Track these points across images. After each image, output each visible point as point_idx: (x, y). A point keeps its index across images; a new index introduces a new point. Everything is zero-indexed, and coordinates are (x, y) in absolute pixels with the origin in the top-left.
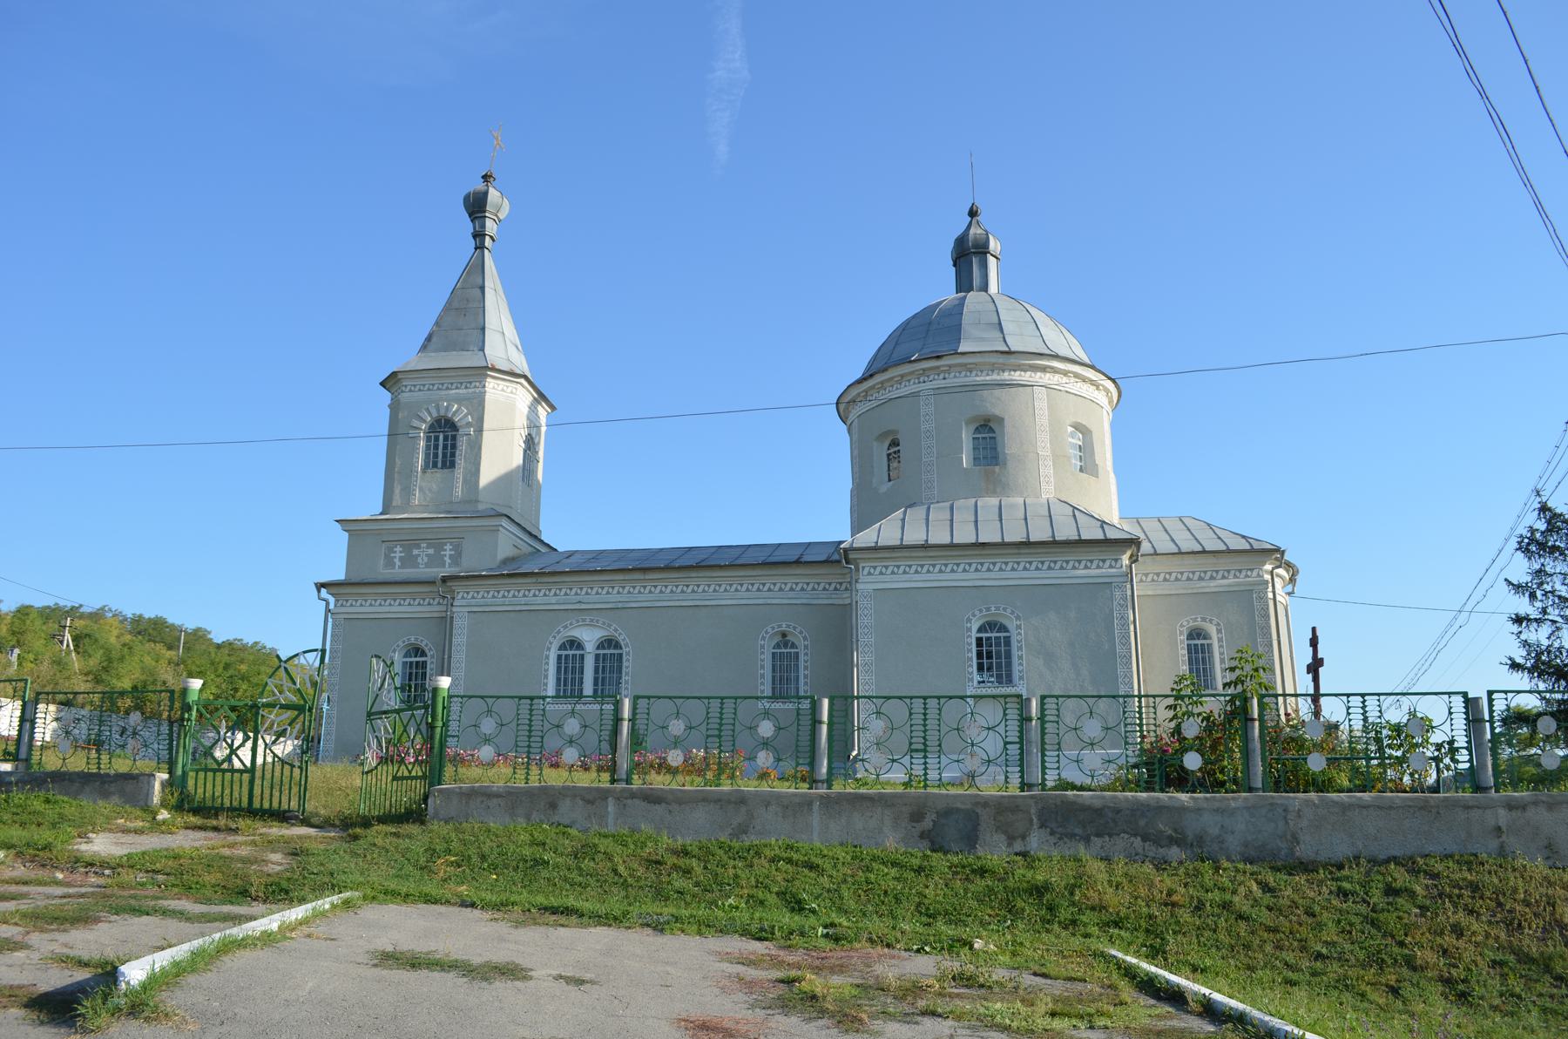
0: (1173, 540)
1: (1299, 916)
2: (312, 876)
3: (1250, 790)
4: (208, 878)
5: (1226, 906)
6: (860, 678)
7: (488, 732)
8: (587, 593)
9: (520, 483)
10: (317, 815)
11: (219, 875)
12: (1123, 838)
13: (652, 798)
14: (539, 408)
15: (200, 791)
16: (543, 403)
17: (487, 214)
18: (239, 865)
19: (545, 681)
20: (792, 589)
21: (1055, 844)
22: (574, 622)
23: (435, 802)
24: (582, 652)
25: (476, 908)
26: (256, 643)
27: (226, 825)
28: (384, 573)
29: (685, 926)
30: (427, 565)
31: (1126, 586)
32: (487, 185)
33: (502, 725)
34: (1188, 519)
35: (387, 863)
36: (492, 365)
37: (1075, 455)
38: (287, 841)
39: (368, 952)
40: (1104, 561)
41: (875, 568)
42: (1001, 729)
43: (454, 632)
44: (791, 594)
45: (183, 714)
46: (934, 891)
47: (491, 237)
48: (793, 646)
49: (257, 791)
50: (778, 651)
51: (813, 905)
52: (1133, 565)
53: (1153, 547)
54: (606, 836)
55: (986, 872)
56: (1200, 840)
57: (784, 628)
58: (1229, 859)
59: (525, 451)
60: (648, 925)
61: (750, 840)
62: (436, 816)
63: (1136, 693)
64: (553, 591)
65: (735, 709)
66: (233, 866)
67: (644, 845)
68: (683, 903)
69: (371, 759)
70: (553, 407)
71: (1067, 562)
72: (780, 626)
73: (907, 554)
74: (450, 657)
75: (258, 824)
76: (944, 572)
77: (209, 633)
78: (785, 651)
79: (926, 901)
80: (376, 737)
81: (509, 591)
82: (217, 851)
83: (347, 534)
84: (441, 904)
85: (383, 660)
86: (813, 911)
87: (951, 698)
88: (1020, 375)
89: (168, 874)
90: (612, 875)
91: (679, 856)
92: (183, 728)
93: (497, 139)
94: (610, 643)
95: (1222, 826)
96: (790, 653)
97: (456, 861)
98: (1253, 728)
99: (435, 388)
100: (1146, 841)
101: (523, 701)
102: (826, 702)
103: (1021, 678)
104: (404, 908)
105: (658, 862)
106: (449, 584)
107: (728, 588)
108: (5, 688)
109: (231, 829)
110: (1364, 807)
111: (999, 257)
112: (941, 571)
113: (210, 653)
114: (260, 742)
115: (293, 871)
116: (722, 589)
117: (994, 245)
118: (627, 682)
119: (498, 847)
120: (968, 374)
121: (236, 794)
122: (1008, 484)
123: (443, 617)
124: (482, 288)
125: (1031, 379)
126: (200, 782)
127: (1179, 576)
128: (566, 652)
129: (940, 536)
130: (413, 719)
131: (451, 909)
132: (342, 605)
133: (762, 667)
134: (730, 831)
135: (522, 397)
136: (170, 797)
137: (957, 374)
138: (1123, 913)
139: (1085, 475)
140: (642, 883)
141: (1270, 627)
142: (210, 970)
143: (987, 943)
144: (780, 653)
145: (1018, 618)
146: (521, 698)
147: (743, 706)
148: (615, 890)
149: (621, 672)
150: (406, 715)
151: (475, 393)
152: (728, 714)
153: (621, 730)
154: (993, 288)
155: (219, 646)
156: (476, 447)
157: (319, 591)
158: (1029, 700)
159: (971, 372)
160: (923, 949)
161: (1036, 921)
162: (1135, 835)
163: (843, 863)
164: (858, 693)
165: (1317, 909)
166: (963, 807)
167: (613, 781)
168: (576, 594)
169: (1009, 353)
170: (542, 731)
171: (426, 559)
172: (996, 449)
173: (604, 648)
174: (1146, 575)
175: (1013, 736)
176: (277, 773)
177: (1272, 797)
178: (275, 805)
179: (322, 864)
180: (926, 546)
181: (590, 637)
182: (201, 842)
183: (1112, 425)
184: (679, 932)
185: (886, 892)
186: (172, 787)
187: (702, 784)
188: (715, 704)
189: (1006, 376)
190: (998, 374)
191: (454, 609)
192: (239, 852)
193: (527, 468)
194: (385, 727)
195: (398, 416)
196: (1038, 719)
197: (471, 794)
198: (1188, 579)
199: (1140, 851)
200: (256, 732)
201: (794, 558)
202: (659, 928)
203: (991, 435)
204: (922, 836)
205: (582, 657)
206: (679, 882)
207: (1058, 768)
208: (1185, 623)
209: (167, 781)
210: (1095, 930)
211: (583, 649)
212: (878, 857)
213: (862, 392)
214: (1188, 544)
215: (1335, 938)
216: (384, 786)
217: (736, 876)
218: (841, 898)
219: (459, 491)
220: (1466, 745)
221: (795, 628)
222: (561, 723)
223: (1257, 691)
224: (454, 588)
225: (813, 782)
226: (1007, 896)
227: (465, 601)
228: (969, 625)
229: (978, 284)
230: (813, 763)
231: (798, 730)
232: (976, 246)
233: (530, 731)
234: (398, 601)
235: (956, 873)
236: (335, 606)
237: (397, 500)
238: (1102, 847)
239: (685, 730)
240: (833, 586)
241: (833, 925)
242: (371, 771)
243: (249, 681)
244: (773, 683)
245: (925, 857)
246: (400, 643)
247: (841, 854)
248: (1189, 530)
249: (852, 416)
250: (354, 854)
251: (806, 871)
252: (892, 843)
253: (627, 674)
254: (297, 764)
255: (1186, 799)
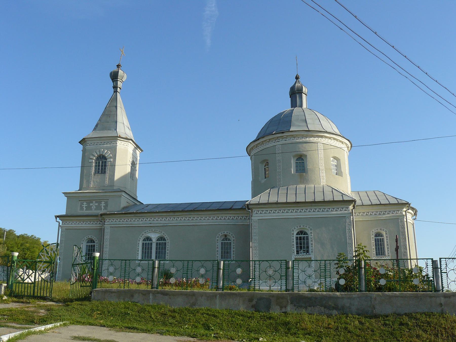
0: (370, 200)
1: (369, 332)
2: (54, 317)
3: (361, 291)
4: (21, 317)
5: (346, 328)
6: (253, 252)
7: (111, 271)
8: (153, 220)
9: (130, 179)
10: (56, 298)
11: (24, 316)
12: (318, 307)
13: (165, 294)
14: (137, 151)
15: (17, 290)
16: (138, 149)
17: (118, 80)
18: (31, 313)
19: (138, 252)
20: (229, 219)
21: (296, 309)
22: (148, 231)
23: (94, 294)
24: (151, 242)
25: (105, 327)
26: (32, 236)
27: (26, 301)
28: (80, 212)
29: (170, 333)
30: (95, 209)
31: (351, 218)
32: (118, 69)
33: (116, 269)
34: (377, 191)
35: (78, 313)
36: (119, 135)
37: (334, 168)
38: (46, 306)
39: (70, 336)
40: (343, 208)
41: (258, 211)
42: (280, 271)
43: (105, 234)
44: (228, 221)
45: (12, 264)
46: (253, 324)
47: (120, 88)
48: (229, 240)
49: (36, 290)
50: (224, 242)
51: (213, 328)
52: (353, 210)
53: (362, 203)
54: (149, 306)
55: (271, 318)
56: (343, 308)
57: (226, 233)
58: (352, 314)
59: (131, 167)
60: (159, 333)
61: (197, 307)
62: (94, 299)
63: (409, 258)
64: (141, 219)
65: (192, 264)
66: (29, 313)
67: (161, 309)
68: (171, 327)
69: (73, 280)
70: (142, 151)
71: (329, 209)
72: (224, 233)
73: (271, 206)
74: (103, 243)
75: (37, 301)
76: (288, 213)
77: (15, 231)
78: (226, 242)
79: (250, 327)
80: (75, 272)
81: (125, 219)
82: (23, 309)
83: (66, 198)
84: (94, 326)
85: (78, 247)
86: (212, 330)
87: (263, 261)
88: (313, 139)
89: (8, 316)
90: (150, 318)
91: (172, 312)
92: (12, 269)
93: (122, 52)
94: (161, 238)
95: (350, 303)
96: (228, 242)
97: (100, 313)
98: (362, 271)
99: (99, 144)
100: (325, 308)
101: (123, 261)
102: (222, 262)
103: (312, 252)
104: (82, 326)
105: (165, 314)
106: (103, 216)
107: (205, 218)
108: (171, 281)
109: (27, 302)
110: (397, 297)
111: (307, 94)
112: (283, 212)
113: (15, 239)
114: (37, 273)
115: (48, 315)
116: (203, 219)
117: (304, 90)
118: (168, 253)
119: (114, 309)
120: (294, 139)
121: (29, 291)
122: (308, 179)
123: (101, 229)
124: (116, 107)
125: (317, 141)
126: (17, 287)
127: (372, 213)
128: (146, 242)
129: (282, 199)
130: (87, 267)
131: (97, 327)
132: (65, 224)
133: (218, 248)
134: (190, 305)
135: (130, 147)
136: (7, 292)
137: (290, 139)
138: (312, 330)
139: (338, 176)
140: (159, 321)
141: (405, 232)
142: (25, 339)
143: (264, 339)
144: (224, 242)
145: (311, 229)
146: (122, 260)
147: (195, 263)
148: (150, 322)
149: (166, 249)
150: (85, 266)
151: (113, 145)
152: (190, 266)
153: (155, 271)
154: (304, 106)
155: (18, 237)
156: (113, 165)
157: (56, 219)
158: (289, 262)
159: (295, 138)
160: (243, 340)
161: (283, 333)
162: (322, 306)
163: (225, 315)
164: (252, 259)
165: (375, 329)
166: (265, 297)
167: (152, 288)
168: (149, 220)
169: (309, 131)
170: (321, 280)
171: (95, 207)
172: (304, 166)
173: (159, 240)
174: (360, 213)
175: (284, 274)
176: (43, 284)
177: (367, 294)
178: (42, 295)
179: (57, 313)
180: (277, 203)
181: (154, 236)
182: (18, 307)
183: (349, 157)
184: (168, 335)
185: (237, 324)
186: (8, 288)
187: (181, 289)
188: (186, 262)
189: (308, 139)
190: (305, 139)
191: (105, 226)
192: (30, 309)
193: (132, 173)
194: (78, 270)
195: (85, 154)
196: (292, 268)
197: (106, 292)
198: (375, 214)
199: (323, 311)
200: (36, 270)
201: (229, 207)
202: (161, 334)
203: (303, 161)
204: (252, 307)
205: (151, 243)
206: (171, 320)
207: (298, 284)
208: (374, 231)
209: (6, 286)
210: (301, 336)
211: (152, 241)
212: (237, 313)
213: (255, 145)
214: (375, 202)
215: (378, 339)
216: (77, 289)
217: (190, 319)
218: (222, 326)
219: (107, 182)
220: (432, 276)
221: (230, 233)
222: (135, 268)
223: (363, 258)
224: (105, 218)
225: (217, 288)
226: (276, 325)
227: (109, 223)
228: (293, 232)
229: (299, 104)
230: (217, 282)
231: (213, 272)
232: (298, 90)
233: (125, 271)
234: (85, 222)
235: (262, 319)
236: (62, 224)
237: (85, 185)
238: (311, 310)
239: (176, 271)
240: (244, 218)
241: (217, 334)
242: (73, 284)
243: (30, 250)
244: (222, 254)
245: (253, 313)
246: (85, 238)
247: (225, 312)
248: (376, 196)
249: (252, 154)
250: (67, 310)
251: (213, 317)
252: (242, 309)
253: (168, 250)
254: (49, 281)
255: (338, 294)
